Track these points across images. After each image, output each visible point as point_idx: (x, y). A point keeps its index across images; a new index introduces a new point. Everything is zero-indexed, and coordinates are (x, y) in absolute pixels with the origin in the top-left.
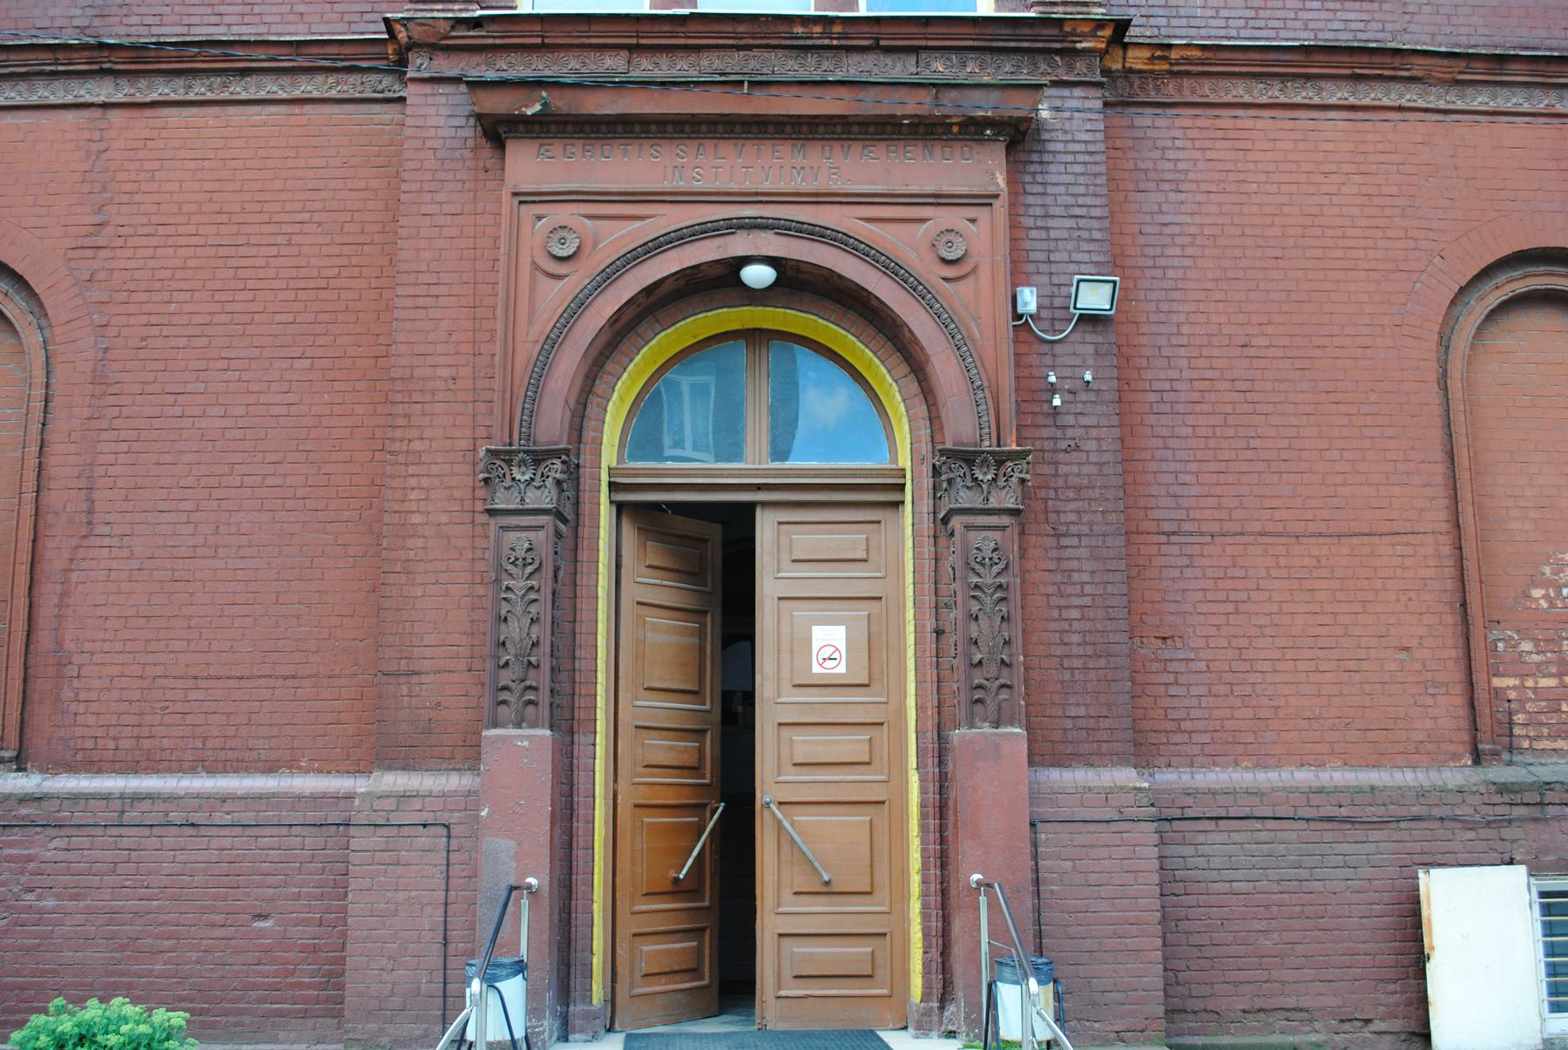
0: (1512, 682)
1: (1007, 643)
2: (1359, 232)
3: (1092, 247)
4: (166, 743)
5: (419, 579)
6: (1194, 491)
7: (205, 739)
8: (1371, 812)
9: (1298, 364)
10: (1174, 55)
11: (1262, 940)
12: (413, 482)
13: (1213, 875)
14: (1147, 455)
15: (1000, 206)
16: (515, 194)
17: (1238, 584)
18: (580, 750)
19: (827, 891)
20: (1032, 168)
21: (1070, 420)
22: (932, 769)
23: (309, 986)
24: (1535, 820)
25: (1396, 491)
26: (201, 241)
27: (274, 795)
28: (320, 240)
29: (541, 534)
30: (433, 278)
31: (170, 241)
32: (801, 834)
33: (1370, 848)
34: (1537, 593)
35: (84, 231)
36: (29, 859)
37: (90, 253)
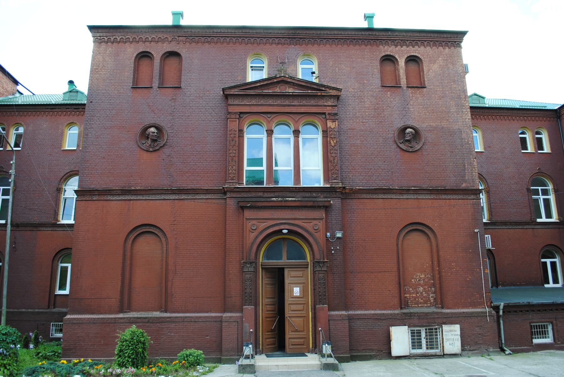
0: (408, 295)
1: (325, 292)
2: (384, 220)
3: (339, 225)
4: (190, 308)
5: (232, 281)
6: (355, 265)
7: (196, 307)
8: (383, 318)
9: (373, 243)
10: (353, 190)
11: (365, 338)
12: (230, 266)
13: (358, 328)
14: (348, 259)
15: (324, 220)
16: (246, 219)
17: (362, 280)
18: (257, 309)
19: (297, 331)
20: (330, 212)
21: (335, 255)
22: (313, 312)
23: (215, 347)
24: (410, 319)
25: (389, 264)
26: (192, 223)
27: (208, 317)
28: (212, 223)
29: (251, 275)
30: (232, 232)
31: (187, 223)
32: (292, 322)
33: (383, 323)
34: (413, 280)
35: (172, 221)
36: (169, 327)
37: (173, 225)
